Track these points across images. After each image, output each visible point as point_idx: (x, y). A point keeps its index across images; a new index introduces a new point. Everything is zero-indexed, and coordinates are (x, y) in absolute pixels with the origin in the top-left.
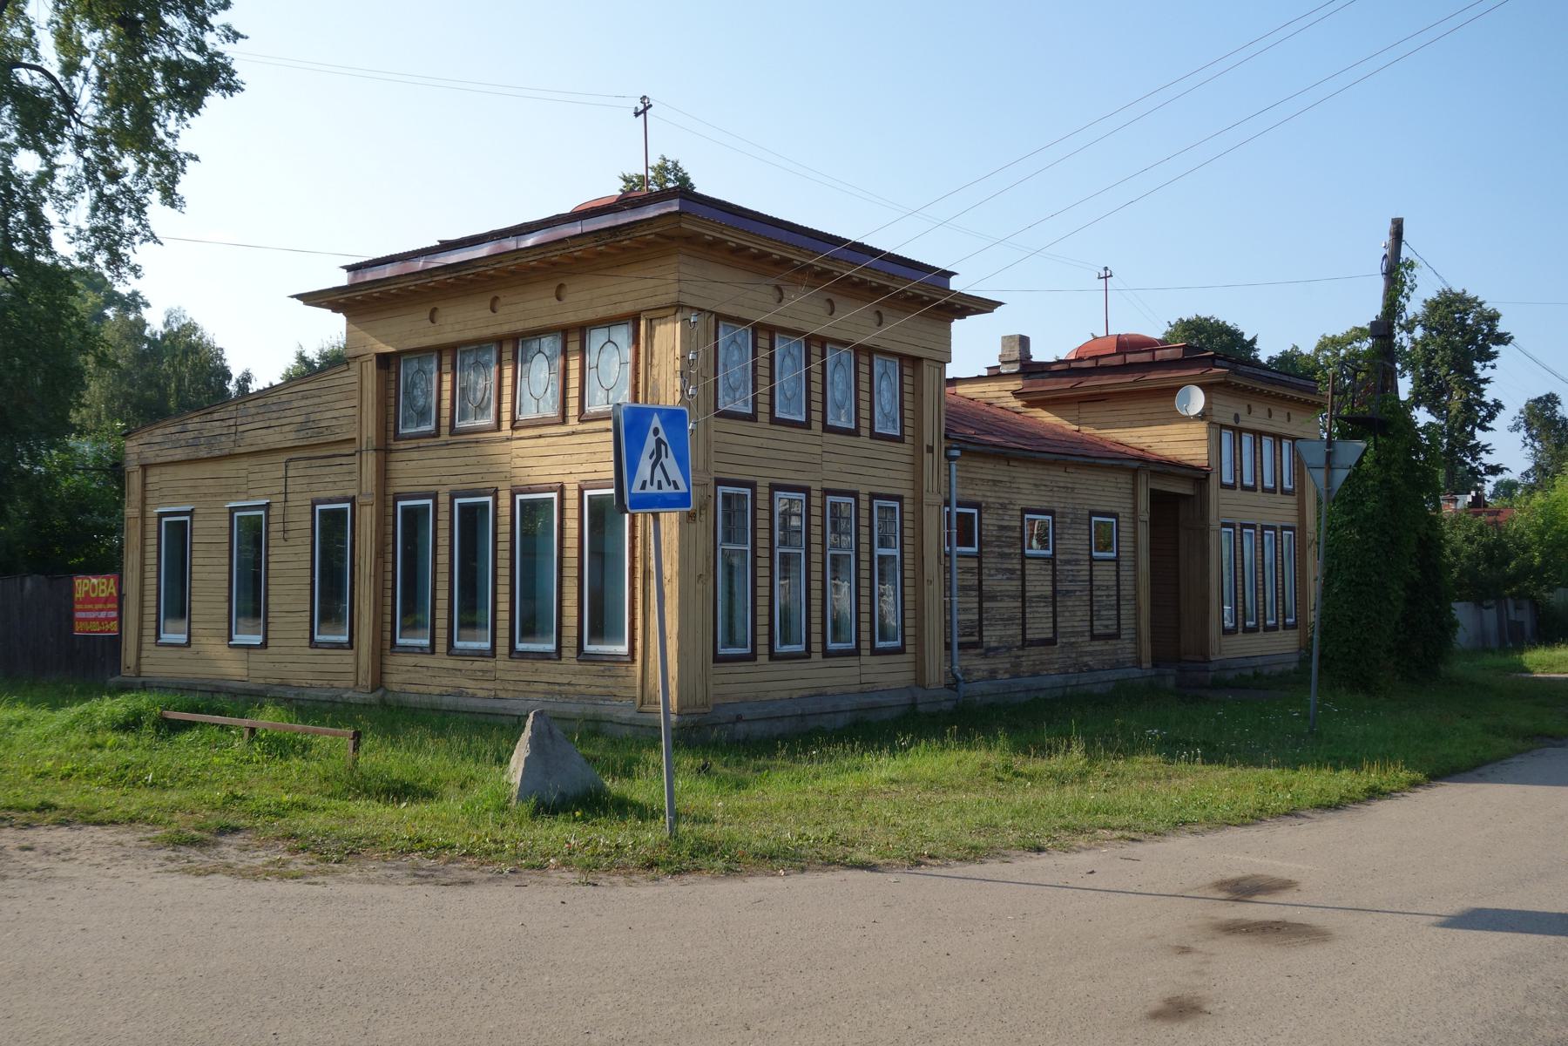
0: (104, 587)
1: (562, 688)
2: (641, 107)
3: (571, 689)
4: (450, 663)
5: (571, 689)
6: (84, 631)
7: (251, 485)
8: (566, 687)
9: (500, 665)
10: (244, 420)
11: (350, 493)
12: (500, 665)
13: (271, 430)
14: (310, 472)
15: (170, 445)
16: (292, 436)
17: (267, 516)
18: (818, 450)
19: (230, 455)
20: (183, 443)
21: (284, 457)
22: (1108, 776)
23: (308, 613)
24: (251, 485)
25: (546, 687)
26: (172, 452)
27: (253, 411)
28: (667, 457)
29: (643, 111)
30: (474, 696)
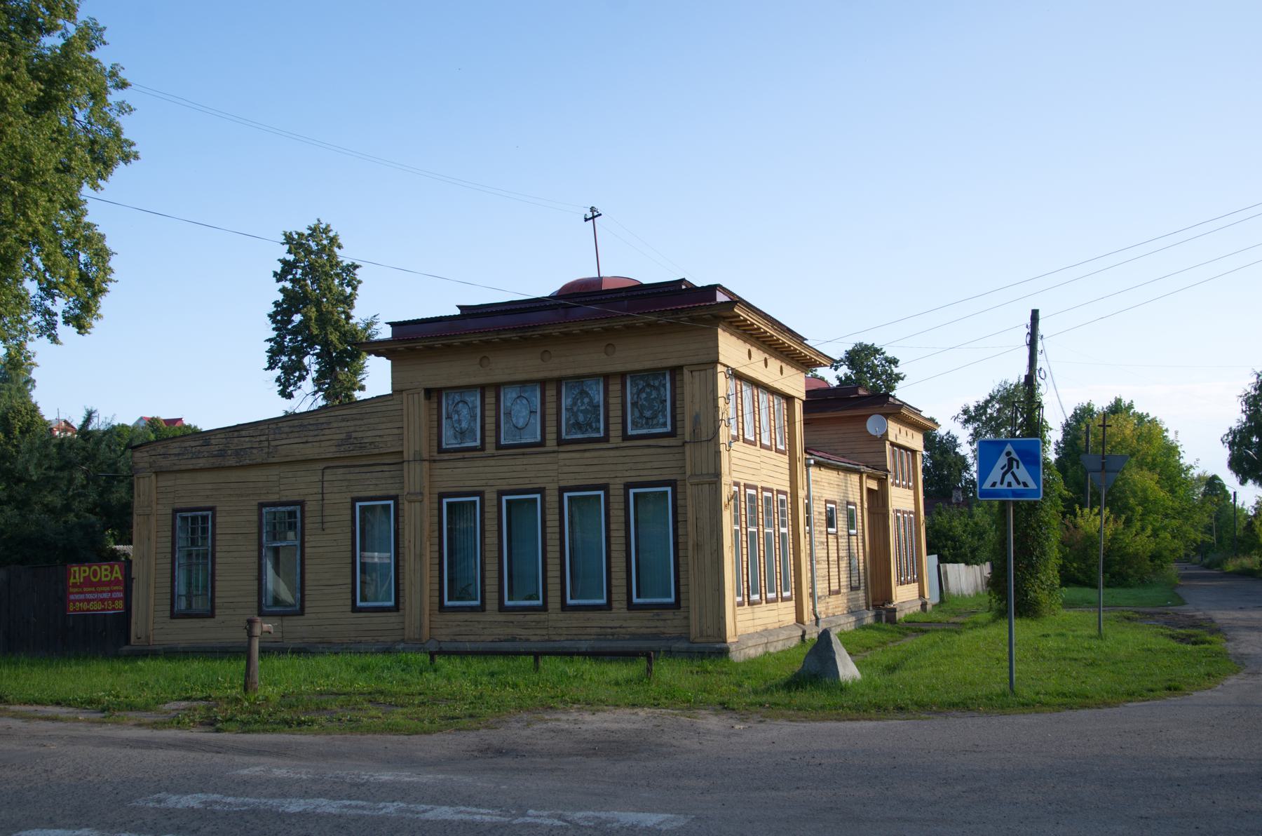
0: (108, 573)
1: (614, 630)
2: (590, 215)
3: (623, 631)
4: (501, 617)
5: (623, 631)
6: (80, 610)
7: (282, 487)
8: (618, 630)
9: (553, 617)
10: (278, 436)
11: (393, 493)
12: (553, 617)
13: (310, 445)
14: (348, 477)
15: (190, 456)
16: (334, 449)
17: (303, 512)
18: (758, 460)
19: (263, 464)
20: (206, 454)
21: (323, 465)
22: (15, 679)
23: (350, 586)
24: (282, 487)
25: (598, 630)
26: (194, 461)
27: (287, 429)
28: (1018, 467)
29: (594, 215)
30: (527, 640)
